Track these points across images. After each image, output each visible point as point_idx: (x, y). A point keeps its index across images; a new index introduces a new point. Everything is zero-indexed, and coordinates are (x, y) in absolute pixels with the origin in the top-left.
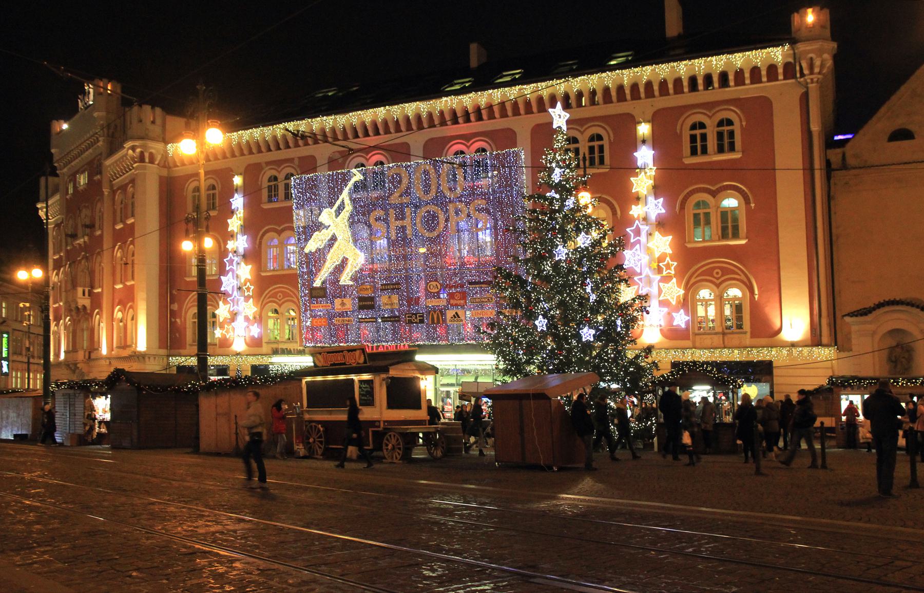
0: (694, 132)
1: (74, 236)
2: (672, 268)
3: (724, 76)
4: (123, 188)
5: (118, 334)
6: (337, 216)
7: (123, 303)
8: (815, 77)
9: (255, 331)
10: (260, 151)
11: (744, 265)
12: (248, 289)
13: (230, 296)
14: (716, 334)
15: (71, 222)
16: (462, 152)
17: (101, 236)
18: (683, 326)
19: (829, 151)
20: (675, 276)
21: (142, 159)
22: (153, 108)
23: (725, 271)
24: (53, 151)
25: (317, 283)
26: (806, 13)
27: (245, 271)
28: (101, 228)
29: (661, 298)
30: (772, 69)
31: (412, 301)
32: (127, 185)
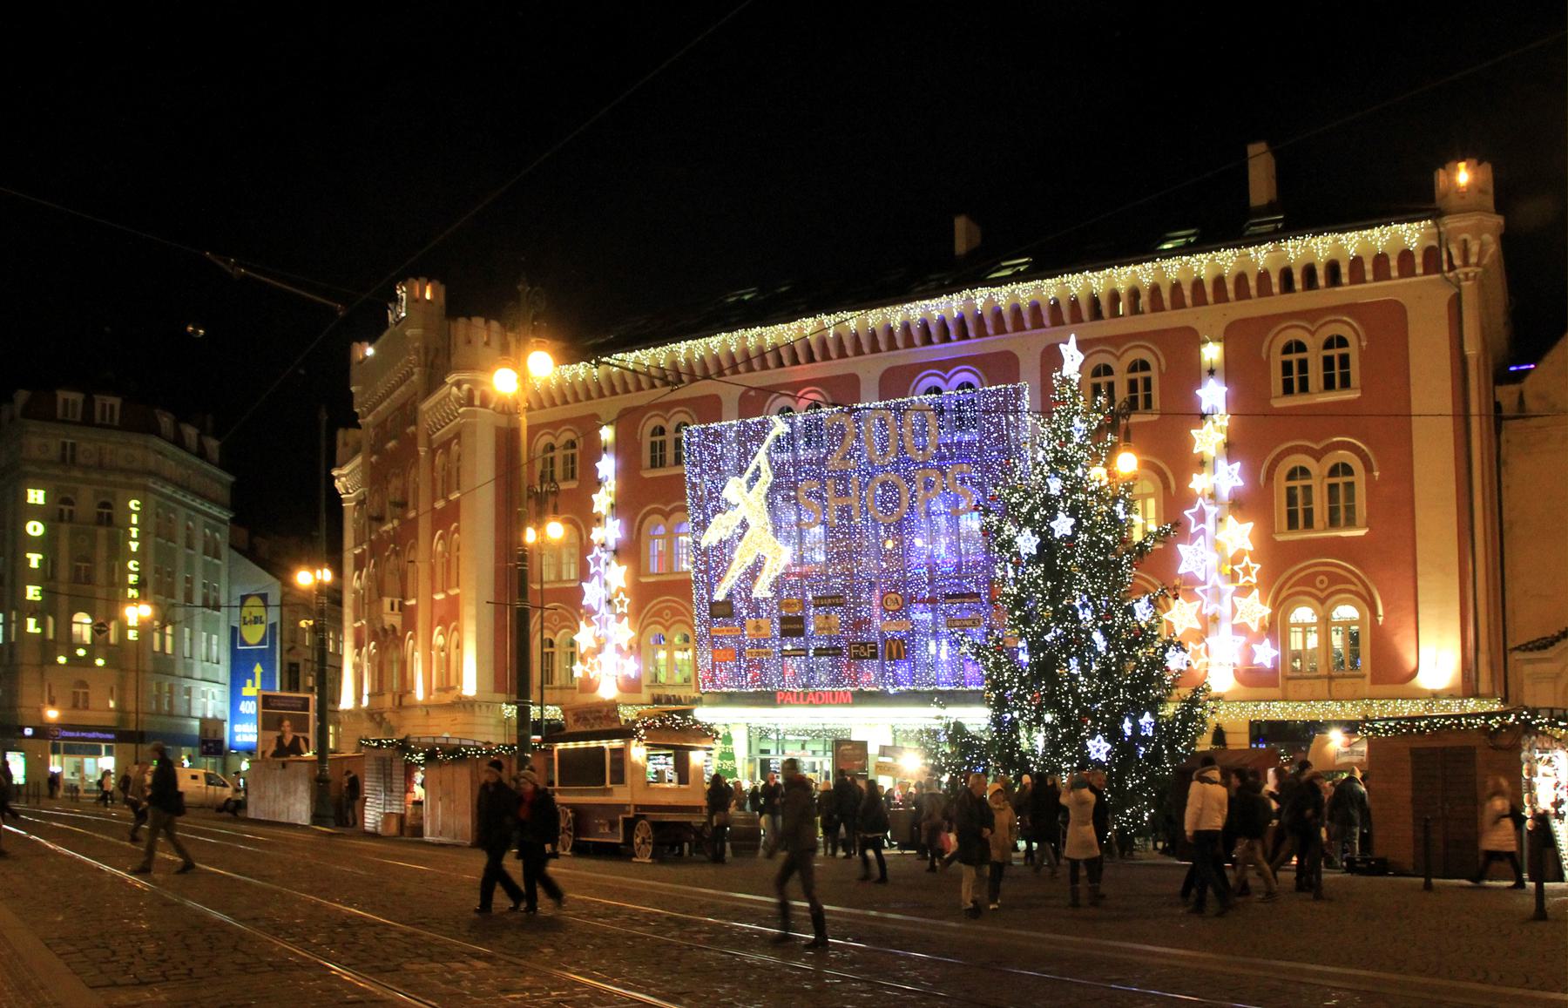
0: (1288, 357)
1: (380, 519)
2: (1253, 573)
3: (1333, 268)
4: (446, 445)
5: (439, 667)
6: (750, 488)
7: (444, 622)
8: (1471, 271)
9: (631, 667)
10: (589, 397)
11: (1365, 573)
12: (621, 603)
13: (595, 613)
14: (1318, 677)
15: (376, 498)
16: (970, 386)
17: (415, 520)
18: (1269, 665)
19: (1499, 389)
20: (1257, 585)
21: (470, 401)
22: (487, 322)
23: (1334, 579)
24: (353, 389)
25: (720, 595)
26: (1456, 169)
27: (617, 575)
28: (416, 508)
29: (1236, 621)
30: (1406, 256)
31: (859, 624)
32: (449, 442)
